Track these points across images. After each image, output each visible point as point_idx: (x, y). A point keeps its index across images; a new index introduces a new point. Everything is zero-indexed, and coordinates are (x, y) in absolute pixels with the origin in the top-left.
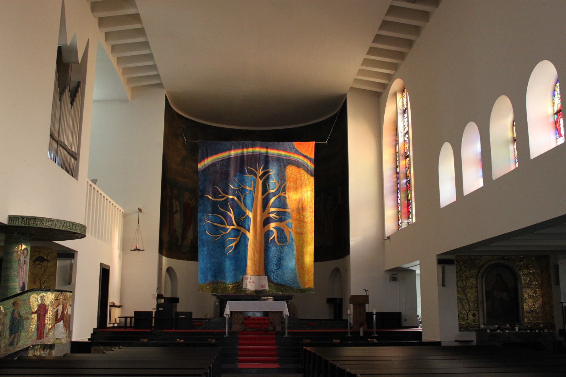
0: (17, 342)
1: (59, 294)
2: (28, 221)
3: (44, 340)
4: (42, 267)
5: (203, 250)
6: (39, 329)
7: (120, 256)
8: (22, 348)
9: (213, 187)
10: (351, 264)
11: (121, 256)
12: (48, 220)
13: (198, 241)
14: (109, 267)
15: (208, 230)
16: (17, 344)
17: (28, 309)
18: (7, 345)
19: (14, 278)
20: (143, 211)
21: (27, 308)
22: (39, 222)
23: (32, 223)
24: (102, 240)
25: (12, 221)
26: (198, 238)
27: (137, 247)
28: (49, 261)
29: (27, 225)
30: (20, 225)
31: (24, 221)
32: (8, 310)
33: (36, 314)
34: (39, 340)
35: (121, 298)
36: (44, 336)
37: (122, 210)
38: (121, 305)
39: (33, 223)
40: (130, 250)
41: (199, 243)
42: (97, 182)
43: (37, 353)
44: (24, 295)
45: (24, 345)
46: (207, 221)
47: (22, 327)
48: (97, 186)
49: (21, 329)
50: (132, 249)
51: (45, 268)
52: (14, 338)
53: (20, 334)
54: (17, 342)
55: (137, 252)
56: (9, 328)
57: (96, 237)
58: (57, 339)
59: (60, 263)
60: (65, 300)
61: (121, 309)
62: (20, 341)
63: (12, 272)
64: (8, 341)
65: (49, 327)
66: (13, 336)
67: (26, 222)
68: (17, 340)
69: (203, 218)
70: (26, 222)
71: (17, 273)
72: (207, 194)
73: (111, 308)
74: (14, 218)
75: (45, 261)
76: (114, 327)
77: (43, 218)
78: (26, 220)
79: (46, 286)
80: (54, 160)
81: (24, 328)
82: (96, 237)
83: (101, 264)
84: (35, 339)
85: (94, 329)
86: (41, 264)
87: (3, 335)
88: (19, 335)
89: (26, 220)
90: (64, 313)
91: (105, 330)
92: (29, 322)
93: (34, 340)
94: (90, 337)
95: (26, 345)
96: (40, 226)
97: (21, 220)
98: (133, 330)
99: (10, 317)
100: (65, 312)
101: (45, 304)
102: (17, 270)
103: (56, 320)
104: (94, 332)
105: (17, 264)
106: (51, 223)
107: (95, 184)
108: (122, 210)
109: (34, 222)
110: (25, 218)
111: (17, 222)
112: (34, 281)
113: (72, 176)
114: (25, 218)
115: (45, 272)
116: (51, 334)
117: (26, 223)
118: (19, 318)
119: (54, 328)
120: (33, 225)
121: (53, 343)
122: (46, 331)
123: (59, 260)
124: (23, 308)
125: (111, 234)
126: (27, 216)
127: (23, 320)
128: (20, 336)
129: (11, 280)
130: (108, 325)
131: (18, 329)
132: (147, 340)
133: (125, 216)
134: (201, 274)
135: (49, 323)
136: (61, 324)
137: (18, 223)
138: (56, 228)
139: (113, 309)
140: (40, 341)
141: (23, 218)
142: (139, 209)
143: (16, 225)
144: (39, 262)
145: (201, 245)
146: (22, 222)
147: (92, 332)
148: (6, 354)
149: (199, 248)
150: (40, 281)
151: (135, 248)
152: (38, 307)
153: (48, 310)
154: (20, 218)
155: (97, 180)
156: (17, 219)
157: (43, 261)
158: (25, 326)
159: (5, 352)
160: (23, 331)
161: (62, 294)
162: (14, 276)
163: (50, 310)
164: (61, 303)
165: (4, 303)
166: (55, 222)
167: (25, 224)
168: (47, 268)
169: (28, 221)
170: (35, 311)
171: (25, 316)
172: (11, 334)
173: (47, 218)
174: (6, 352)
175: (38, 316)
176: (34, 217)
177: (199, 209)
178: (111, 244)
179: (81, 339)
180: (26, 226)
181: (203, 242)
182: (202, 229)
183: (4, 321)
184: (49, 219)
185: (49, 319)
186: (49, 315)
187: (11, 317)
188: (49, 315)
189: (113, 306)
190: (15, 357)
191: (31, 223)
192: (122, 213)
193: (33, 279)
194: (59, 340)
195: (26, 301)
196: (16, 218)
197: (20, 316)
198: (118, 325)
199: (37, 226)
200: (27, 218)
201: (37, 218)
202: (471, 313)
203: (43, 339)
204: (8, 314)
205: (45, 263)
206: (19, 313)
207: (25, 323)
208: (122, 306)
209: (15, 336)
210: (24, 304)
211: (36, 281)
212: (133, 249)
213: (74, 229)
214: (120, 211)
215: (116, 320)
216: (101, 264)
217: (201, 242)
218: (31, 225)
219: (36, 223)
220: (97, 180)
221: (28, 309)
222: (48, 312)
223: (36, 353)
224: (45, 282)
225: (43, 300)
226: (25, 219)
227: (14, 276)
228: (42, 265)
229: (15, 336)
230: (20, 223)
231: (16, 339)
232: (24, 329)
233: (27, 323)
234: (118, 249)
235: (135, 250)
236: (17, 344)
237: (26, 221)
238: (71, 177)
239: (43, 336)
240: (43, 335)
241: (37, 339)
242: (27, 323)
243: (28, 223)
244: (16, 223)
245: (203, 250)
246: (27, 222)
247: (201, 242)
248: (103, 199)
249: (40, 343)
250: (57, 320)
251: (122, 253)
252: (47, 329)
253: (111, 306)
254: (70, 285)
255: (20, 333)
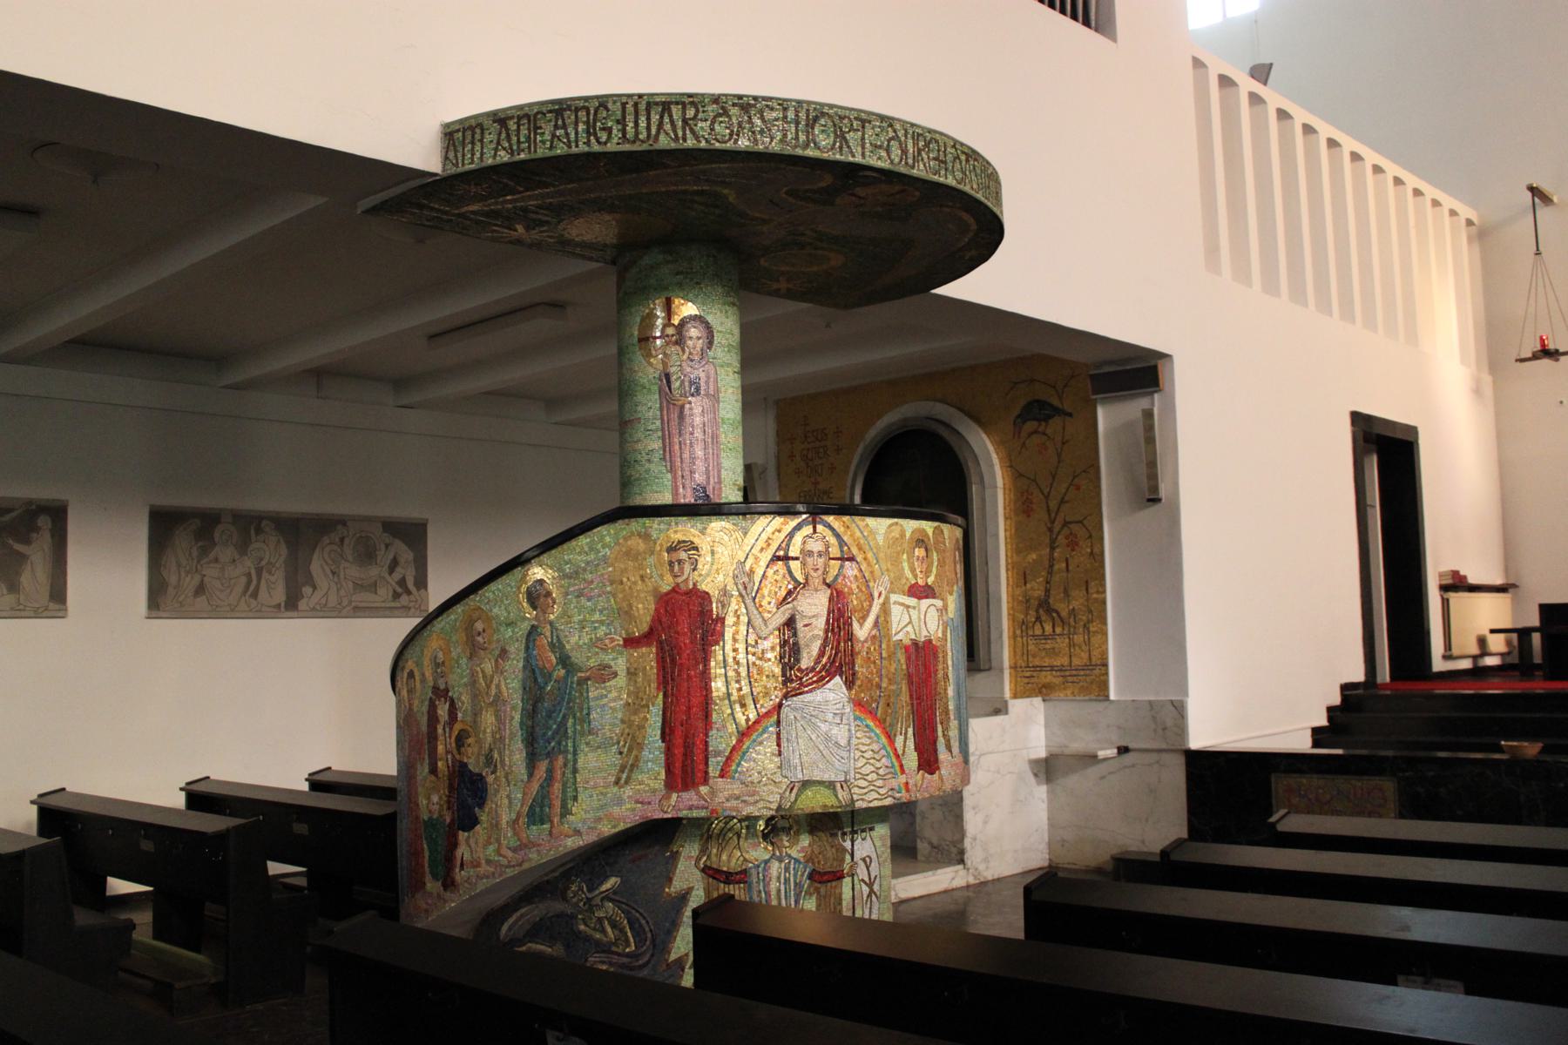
0: (564, 805)
1: (798, 527)
2: (524, 132)
3: (713, 793)
4: (1048, 443)
6: (672, 731)
7: (1477, 391)
8: (590, 838)
10: (1220, 845)
11: (1488, 390)
12: (636, 105)
14: (1413, 430)
16: (563, 815)
17: (602, 622)
18: (519, 815)
19: (647, 471)
20: (1555, 199)
21: (597, 616)
22: (581, 127)
23: (548, 137)
24: (1347, 314)
25: (456, 151)
27: (1543, 345)
28: (1070, 415)
29: (522, 156)
30: (490, 162)
31: (508, 138)
32: (509, 632)
33: (649, 645)
34: (685, 795)
35: (1509, 551)
36: (714, 770)
37: (1466, 212)
38: (1510, 582)
39: (554, 136)
40: (1517, 360)
42: (1272, 70)
43: (724, 857)
44: (573, 543)
45: (599, 820)
47: (582, 721)
48: (1352, 136)
49: (575, 732)
50: (1523, 356)
52: (550, 778)
53: (575, 761)
54: (564, 805)
55: (1546, 363)
56: (522, 723)
57: (1374, 329)
58: (806, 784)
59: (1106, 417)
60: (852, 559)
61: (1513, 600)
62: (575, 799)
63: (639, 441)
64: (524, 794)
65: (741, 718)
66: (542, 767)
67: (514, 139)
68: (564, 792)
70: (514, 139)
71: (660, 443)
73: (1445, 596)
74: (464, 133)
76: (1478, 672)
77: (603, 102)
78: (515, 127)
79: (1068, 519)
82: (1374, 329)
83: (1357, 418)
84: (659, 784)
85: (1346, 688)
86: (1041, 429)
87: (503, 762)
88: (570, 765)
89: (518, 130)
90: (850, 637)
91: (1422, 687)
92: (614, 694)
93: (654, 791)
94: (1322, 721)
95: (610, 817)
96: (588, 143)
97: (493, 137)
98: (1539, 686)
99: (521, 665)
100: (862, 631)
101: (703, 587)
102: (657, 430)
103: (787, 680)
104: (1344, 698)
105: (657, 396)
106: (655, 118)
107: (1265, 83)
108: (1466, 212)
109: (556, 127)
110: (512, 118)
111: (478, 147)
113: (1086, 23)
114: (512, 118)
115: (1059, 462)
116: (762, 755)
117: (515, 147)
118: (563, 672)
119: (778, 723)
120: (551, 148)
121: (779, 808)
122: (721, 740)
123: (1104, 401)
124: (576, 618)
125: (1409, 298)
126: (520, 107)
127: (583, 682)
128: (575, 771)
129: (638, 479)
130: (1438, 665)
131: (562, 730)
132: (1541, 745)
133: (1481, 234)
135: (735, 693)
136: (831, 696)
137: (482, 154)
138: (690, 143)
139: (1455, 598)
140: (689, 797)
141: (500, 119)
142: (1534, 190)
143: (472, 167)
146: (498, 143)
147: (1336, 700)
148: (520, 865)
150: (1047, 497)
151: (1532, 346)
152: (657, 603)
153: (721, 620)
154: (487, 123)
155: (1271, 64)
156: (478, 131)
157: (1047, 418)
158: (594, 715)
159: (514, 850)
160: (587, 744)
161: (820, 528)
162: (649, 461)
163: (737, 624)
164: (816, 580)
165: (491, 595)
166: (676, 112)
167: (512, 154)
169: (524, 132)
170: (645, 627)
171: (592, 663)
172: (532, 759)
173: (630, 96)
174: (519, 857)
175: (661, 661)
176: (553, 102)
178: (1412, 337)
179: (1243, 736)
180: (517, 158)
183: (498, 686)
184: (640, 96)
185: (738, 674)
186: (735, 650)
187: (524, 666)
188: (735, 650)
189: (1456, 584)
190: (606, 878)
191: (539, 138)
192: (1469, 223)
194: (828, 792)
195: (589, 577)
196: (472, 129)
197: (565, 661)
198: (1503, 660)
199: (574, 150)
200: (519, 118)
201: (569, 108)
203: (704, 789)
204: (512, 649)
206: (557, 646)
207: (597, 699)
208: (1514, 586)
209: (550, 772)
210: (578, 596)
211: (1031, 503)
212: (1530, 355)
213: (824, 141)
214: (1453, 213)
215: (1482, 641)
216: (1357, 418)
218: (541, 152)
219: (567, 134)
220: (1271, 64)
221: (602, 622)
222: (723, 635)
223: (719, 856)
224: (1062, 501)
225: (687, 568)
226: (512, 125)
227: (649, 461)
228: (1044, 434)
229: (550, 772)
230: (492, 154)
231: (557, 786)
232: (590, 733)
233: (602, 697)
234: (1463, 361)
235: (1535, 357)
236: (566, 812)
237: (518, 135)
238: (1078, 27)
239: (706, 773)
240: (707, 764)
241: (671, 785)
242: (605, 701)
243: (528, 139)
244: (473, 155)
246: (522, 139)
248: (1331, 158)
249: (690, 808)
250: (794, 679)
251: (1487, 379)
252: (732, 728)
253: (1445, 588)
254: (1156, 508)
255: (575, 753)
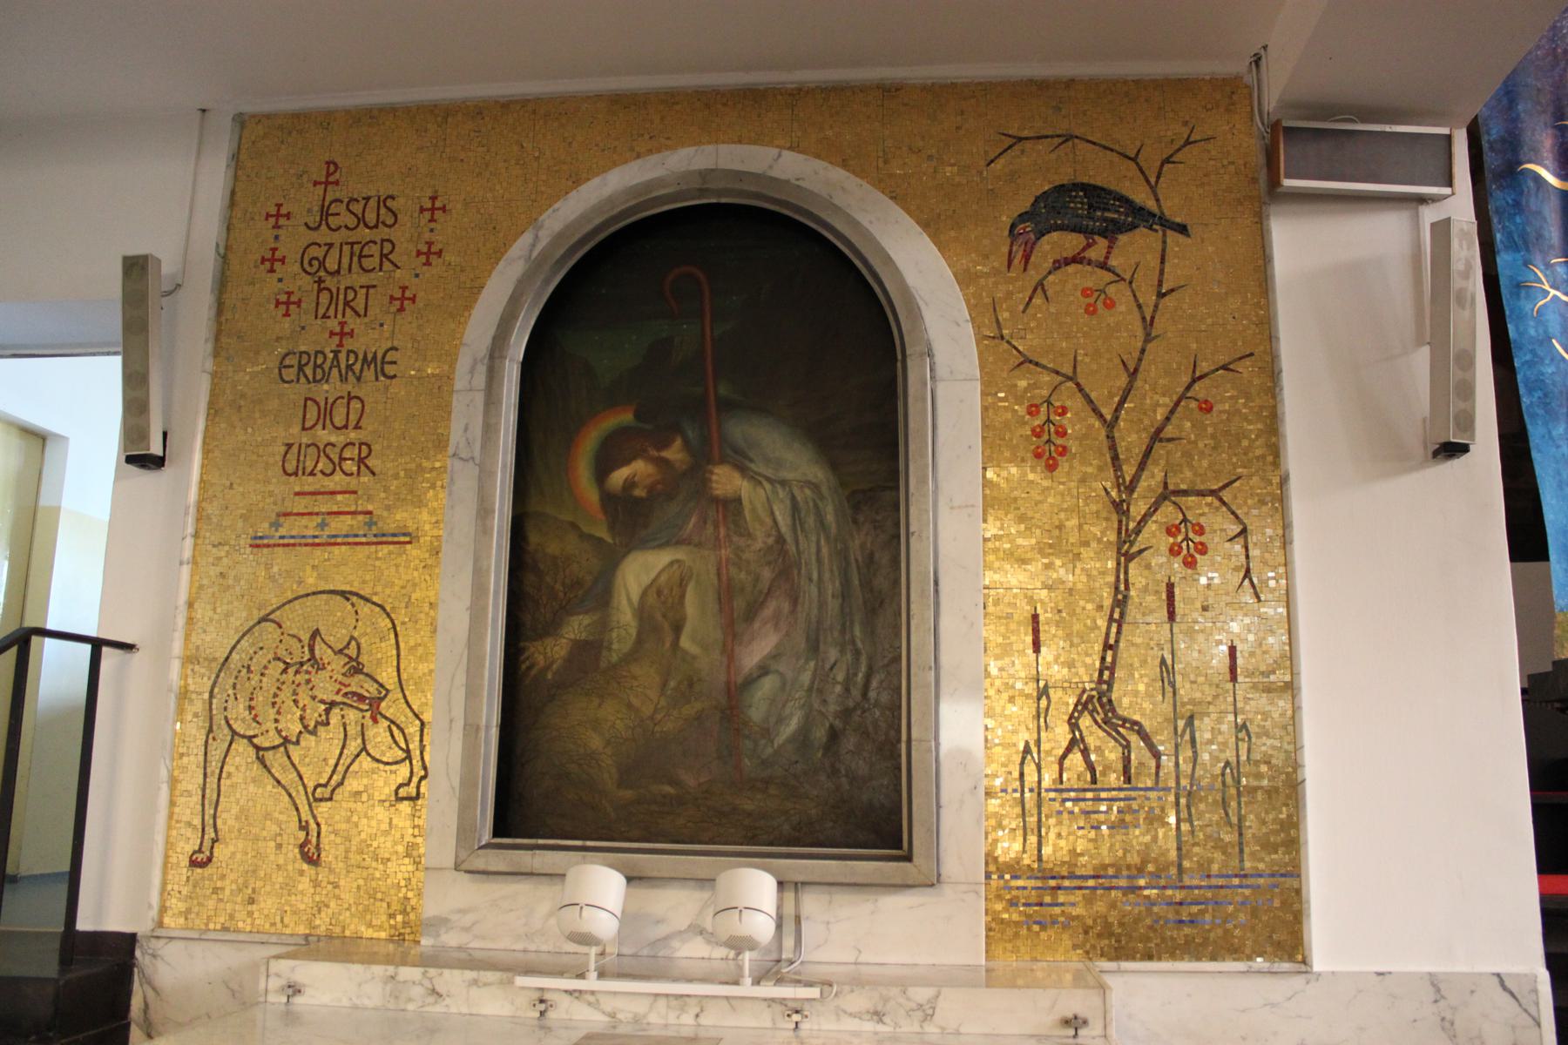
5: (1554, 433)
9: (1555, 127)
13: (1522, 391)
15: (1562, 334)
26: (1519, 377)
28: (1182, 229)
41: (1525, 401)
46: (1553, 292)
51: (1149, 298)
69: (1532, 277)
72: (1530, 162)
75: (1133, 227)
80: (333, 540)
81: (1008, 954)
86: (1094, 254)
112: (1037, 434)
115: (1148, 338)
134: (637, 1020)
144: (1072, 242)
145: (1541, 412)
149: (1529, 427)
157: (1112, 231)
168: (1161, 295)
177: (1498, 236)
181: (1546, 395)
182: (1532, 332)
193: (1033, 410)
202: (1286, 940)
205: (1136, 248)
217: (1539, 394)
228: (1103, 266)
245: (1551, 438)
247: (1539, 394)
